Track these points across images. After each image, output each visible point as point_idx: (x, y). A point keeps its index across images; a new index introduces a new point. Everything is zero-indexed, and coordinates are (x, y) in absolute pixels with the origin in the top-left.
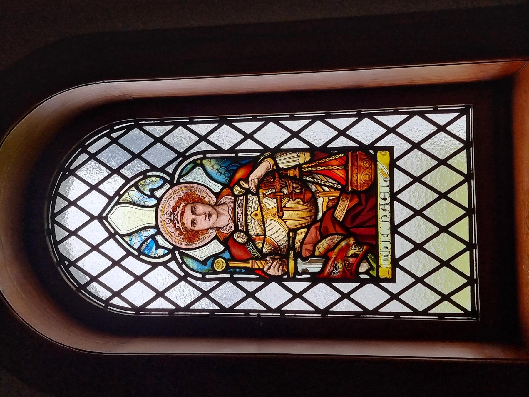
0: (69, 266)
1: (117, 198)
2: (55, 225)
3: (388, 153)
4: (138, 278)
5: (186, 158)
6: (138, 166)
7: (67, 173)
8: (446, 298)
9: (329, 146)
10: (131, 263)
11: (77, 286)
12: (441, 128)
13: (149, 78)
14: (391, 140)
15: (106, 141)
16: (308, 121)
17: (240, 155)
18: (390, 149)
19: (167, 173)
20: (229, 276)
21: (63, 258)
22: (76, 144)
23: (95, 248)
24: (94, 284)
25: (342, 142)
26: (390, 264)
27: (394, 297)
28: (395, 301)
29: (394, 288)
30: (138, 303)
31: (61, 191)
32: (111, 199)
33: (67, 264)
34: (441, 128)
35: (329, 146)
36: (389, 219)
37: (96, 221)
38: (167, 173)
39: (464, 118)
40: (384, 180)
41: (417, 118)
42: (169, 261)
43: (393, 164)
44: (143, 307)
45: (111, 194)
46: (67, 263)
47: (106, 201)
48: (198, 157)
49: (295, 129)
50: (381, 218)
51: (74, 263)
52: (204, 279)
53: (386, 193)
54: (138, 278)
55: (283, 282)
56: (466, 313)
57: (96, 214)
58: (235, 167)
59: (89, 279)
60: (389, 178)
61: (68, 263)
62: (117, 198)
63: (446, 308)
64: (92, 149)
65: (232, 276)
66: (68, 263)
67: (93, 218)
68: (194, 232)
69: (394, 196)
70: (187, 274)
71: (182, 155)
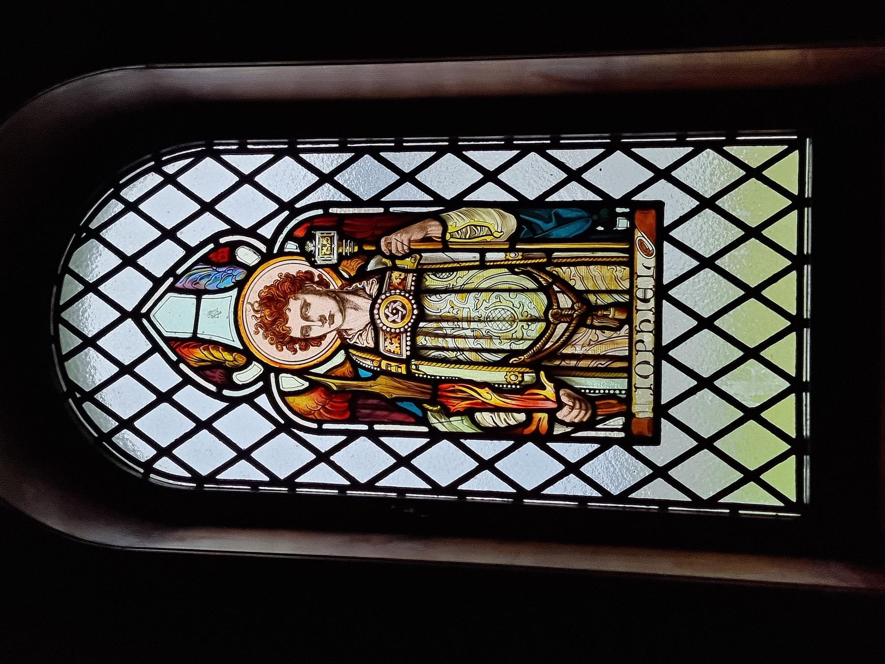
1: (171, 280)
5: (295, 213)
6: (209, 225)
7: (85, 234)
8: (752, 476)
10: (188, 396)
14: (660, 191)
15: (154, 179)
18: (658, 206)
19: (261, 239)
20: (365, 427)
21: (73, 387)
25: (574, 192)
26: (651, 411)
27: (660, 472)
29: (659, 455)
31: (71, 266)
32: (157, 282)
36: (651, 326)
37: (129, 322)
38: (261, 239)
39: (796, 154)
42: (257, 393)
44: (212, 477)
45: (159, 274)
47: (149, 284)
49: (490, 185)
51: (90, 396)
52: (320, 432)
53: (648, 290)
56: (789, 505)
57: (129, 308)
60: (655, 258)
62: (171, 280)
63: (751, 494)
64: (131, 193)
65: (371, 428)
67: (125, 315)
69: (662, 292)
71: (289, 207)
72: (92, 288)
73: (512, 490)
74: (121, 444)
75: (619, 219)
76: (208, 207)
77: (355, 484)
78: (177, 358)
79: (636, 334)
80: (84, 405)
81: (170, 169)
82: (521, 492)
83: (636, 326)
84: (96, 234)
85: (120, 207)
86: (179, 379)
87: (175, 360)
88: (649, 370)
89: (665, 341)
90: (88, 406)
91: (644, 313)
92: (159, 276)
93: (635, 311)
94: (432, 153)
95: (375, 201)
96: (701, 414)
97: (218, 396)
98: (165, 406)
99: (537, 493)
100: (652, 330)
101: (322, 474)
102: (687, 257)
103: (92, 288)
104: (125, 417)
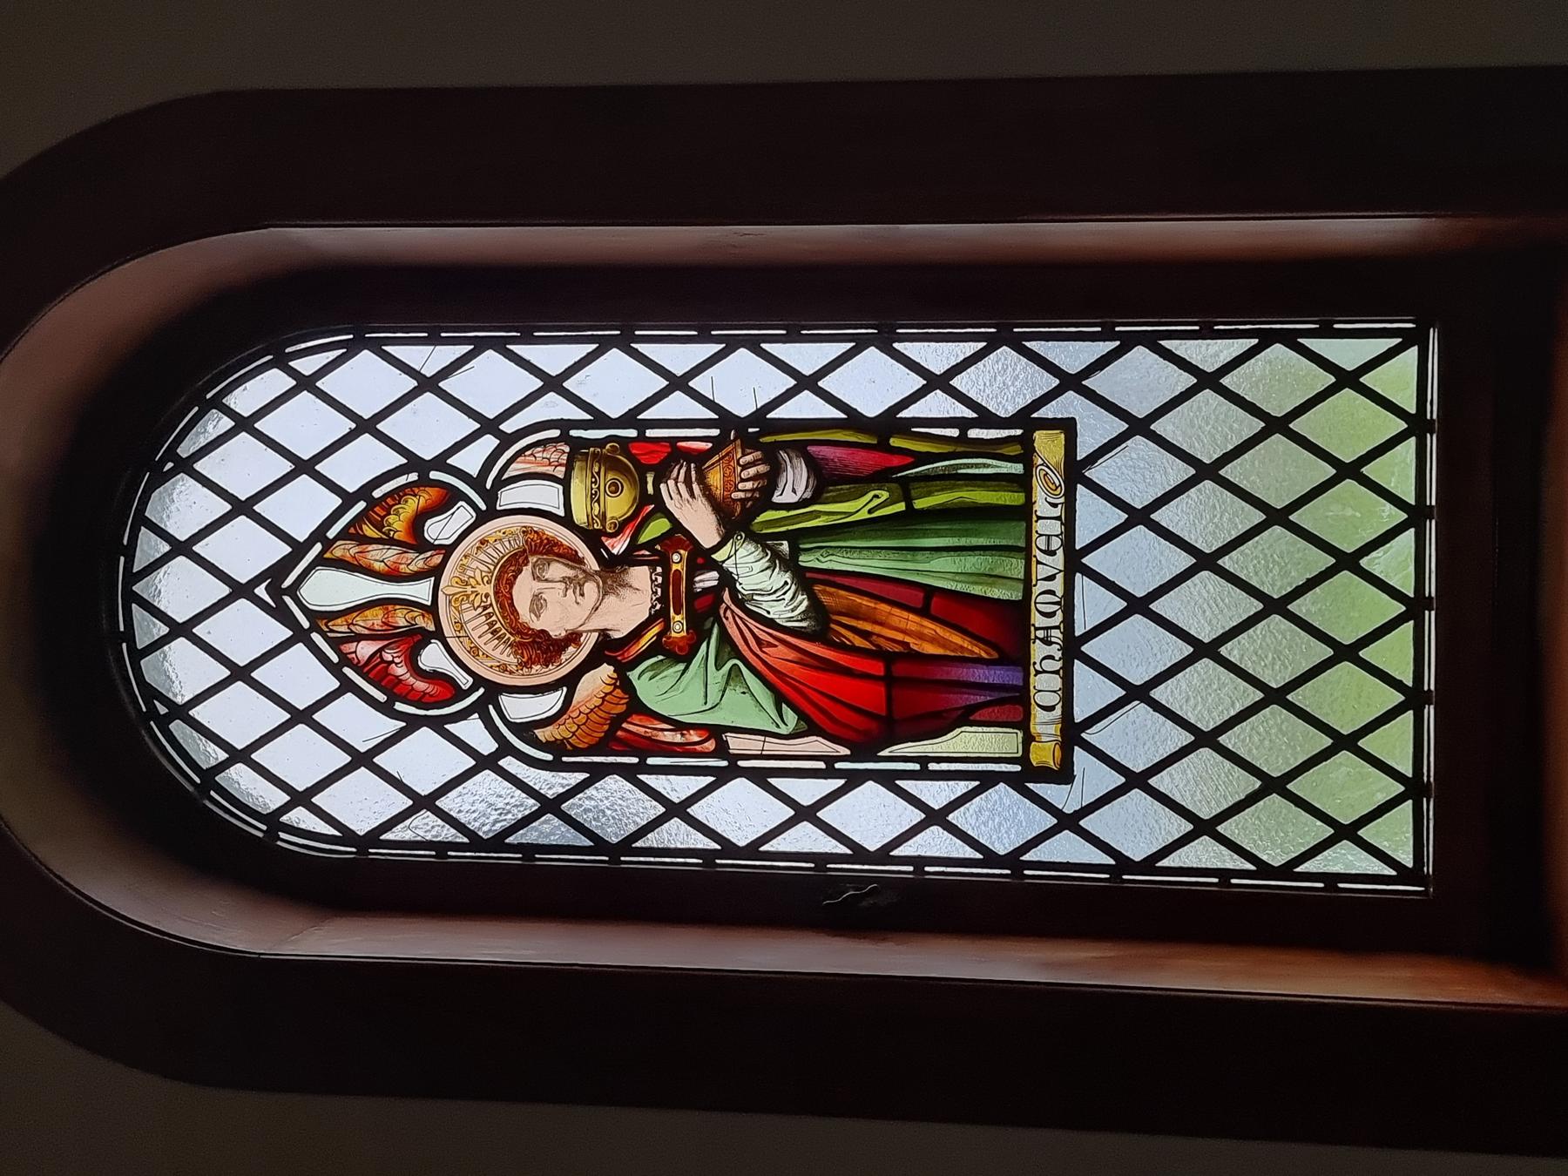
0: (169, 718)
1: (318, 547)
4: (362, 759)
8: (1347, 832)
9: (904, 414)
11: (198, 781)
12: (1347, 379)
13: (1135, 215)
14: (1070, 405)
15: (275, 381)
17: (650, 433)
18: (1068, 426)
21: (151, 693)
23: (302, 717)
24: (240, 767)
27: (1068, 822)
29: (1065, 798)
33: (162, 713)
34: (1347, 379)
35: (904, 414)
39: (1413, 351)
40: (1049, 503)
45: (301, 537)
46: (163, 710)
48: (894, 509)
50: (1038, 663)
51: (181, 712)
54: (362, 759)
55: (769, 780)
56: (1404, 874)
61: (167, 711)
62: (318, 547)
64: (245, 399)
66: (167, 711)
72: (182, 548)
76: (366, 426)
78: (396, 707)
79: (1036, 521)
80: (172, 726)
81: (306, 366)
83: (1035, 663)
85: (227, 423)
86: (335, 684)
87: (397, 703)
90: (177, 727)
91: (1044, 687)
92: (301, 540)
93: (1035, 518)
95: (629, 419)
96: (1206, 441)
97: (386, 709)
98: (424, 789)
100: (1058, 668)
103: (182, 548)
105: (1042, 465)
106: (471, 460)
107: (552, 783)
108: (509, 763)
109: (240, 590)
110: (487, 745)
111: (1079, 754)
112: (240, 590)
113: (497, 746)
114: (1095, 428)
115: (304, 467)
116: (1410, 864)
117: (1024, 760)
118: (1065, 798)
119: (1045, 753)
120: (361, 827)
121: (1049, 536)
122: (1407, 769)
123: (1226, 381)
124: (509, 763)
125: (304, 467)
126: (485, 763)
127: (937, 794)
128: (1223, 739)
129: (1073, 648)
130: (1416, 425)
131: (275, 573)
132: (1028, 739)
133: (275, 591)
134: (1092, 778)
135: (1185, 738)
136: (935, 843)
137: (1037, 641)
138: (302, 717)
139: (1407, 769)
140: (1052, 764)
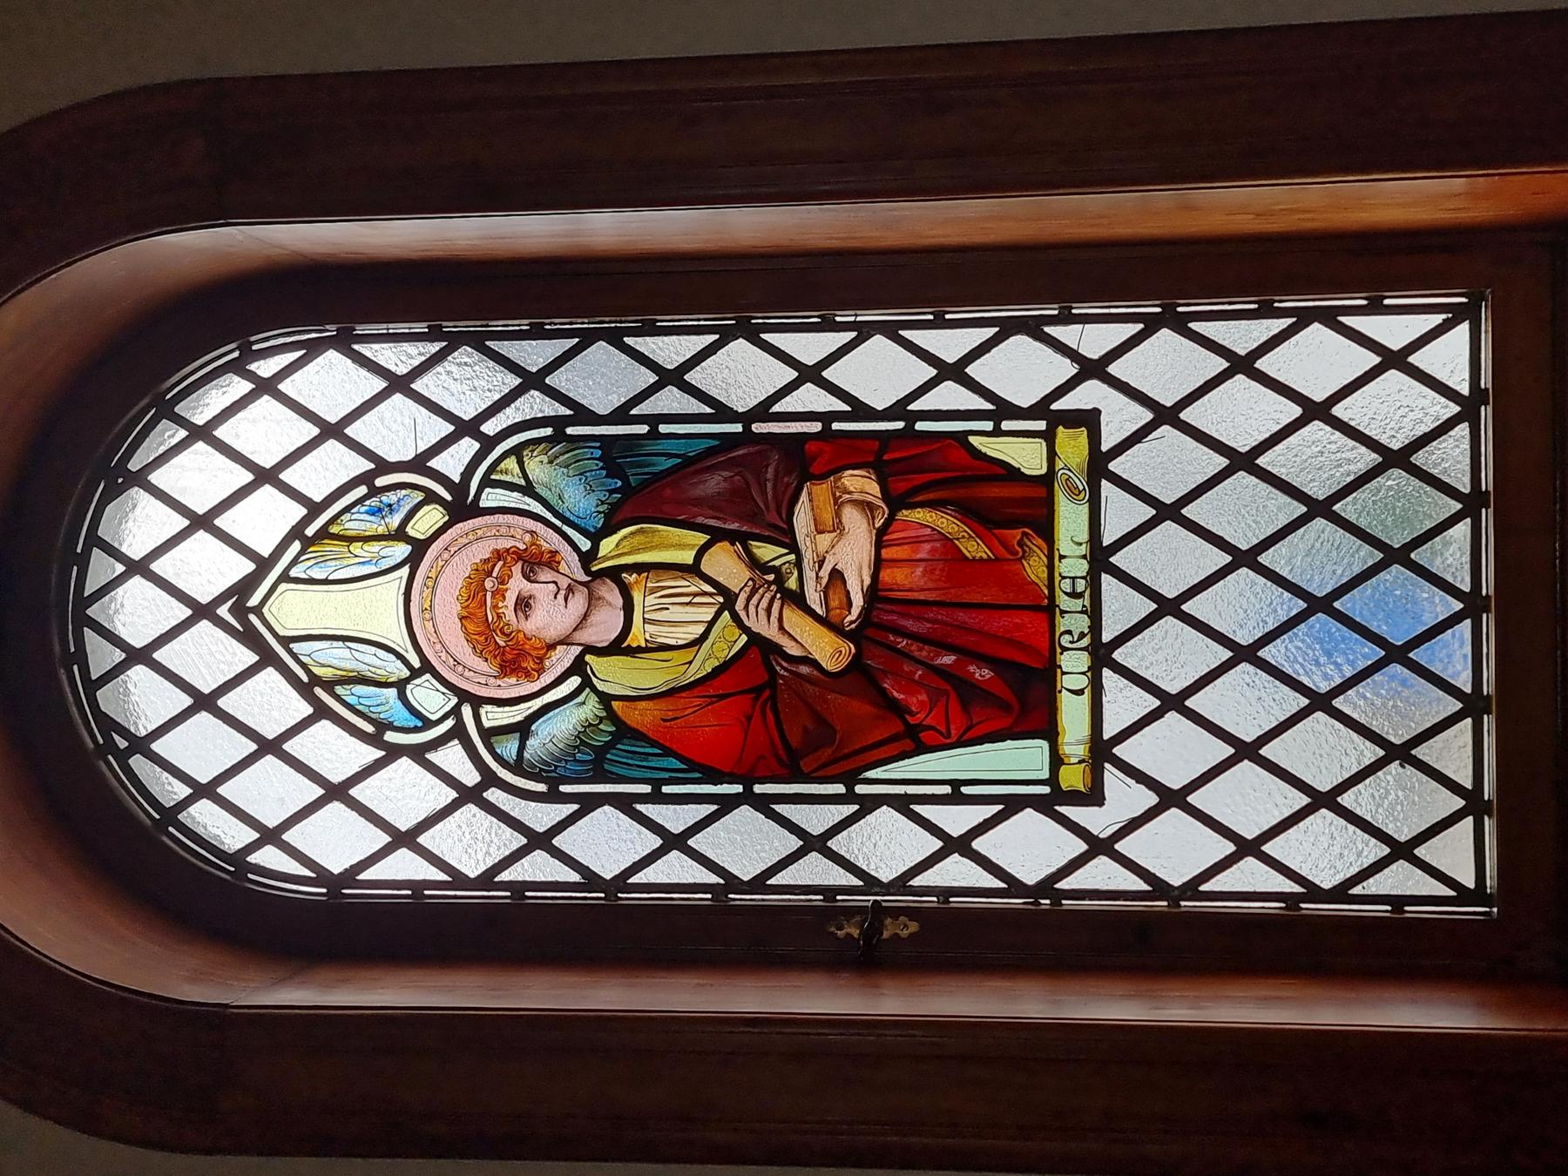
2: (85, 629)
3: (1082, 435)
12: (1394, 360)
14: (1089, 395)
15: (238, 387)
16: (990, 332)
17: (921, 426)
18: (1089, 420)
21: (109, 725)
22: (141, 399)
27: (1099, 847)
28: (1250, 862)
29: (1098, 820)
30: (336, 865)
33: (122, 747)
34: (1394, 360)
39: (1464, 329)
41: (878, 342)
43: (1098, 466)
46: (122, 744)
51: (141, 745)
54: (337, 792)
56: (1463, 895)
58: (888, 458)
59: (187, 791)
60: (1088, 504)
61: (127, 744)
63: (1400, 880)
64: (206, 405)
66: (127, 744)
68: (542, 652)
69: (1100, 558)
70: (489, 779)
72: (139, 567)
73: (713, 879)
74: (188, 823)
75: (1041, 443)
77: (1314, 892)
79: (1061, 654)
80: (131, 761)
82: (732, 882)
84: (140, 479)
86: (307, 710)
88: (1082, 682)
89: (1107, 637)
90: (138, 762)
93: (1059, 650)
94: (992, 331)
95: (621, 415)
99: (759, 883)
101: (675, 869)
102: (1284, 499)
103: (139, 567)
104: (204, 779)
105: (1063, 469)
106: (452, 463)
107: (542, 816)
108: (494, 795)
109: (202, 612)
110: (471, 777)
111: (1107, 580)
112: (202, 612)
113: (479, 779)
114: (1120, 417)
115: (265, 476)
116: (1471, 885)
117: (1053, 781)
118: (1098, 820)
119: (1072, 778)
120: (336, 868)
121: (1073, 578)
122: (1464, 682)
123: (1262, 461)
124: (494, 795)
125: (265, 476)
126: (468, 795)
127: (957, 820)
128: (1267, 848)
129: (1102, 656)
130: (1471, 504)
131: (244, 587)
132: (1057, 761)
133: (240, 611)
134: (1122, 798)
135: (1224, 559)
136: (956, 872)
137: (1064, 690)
138: (269, 747)
139: (1464, 682)
140: (1082, 786)
